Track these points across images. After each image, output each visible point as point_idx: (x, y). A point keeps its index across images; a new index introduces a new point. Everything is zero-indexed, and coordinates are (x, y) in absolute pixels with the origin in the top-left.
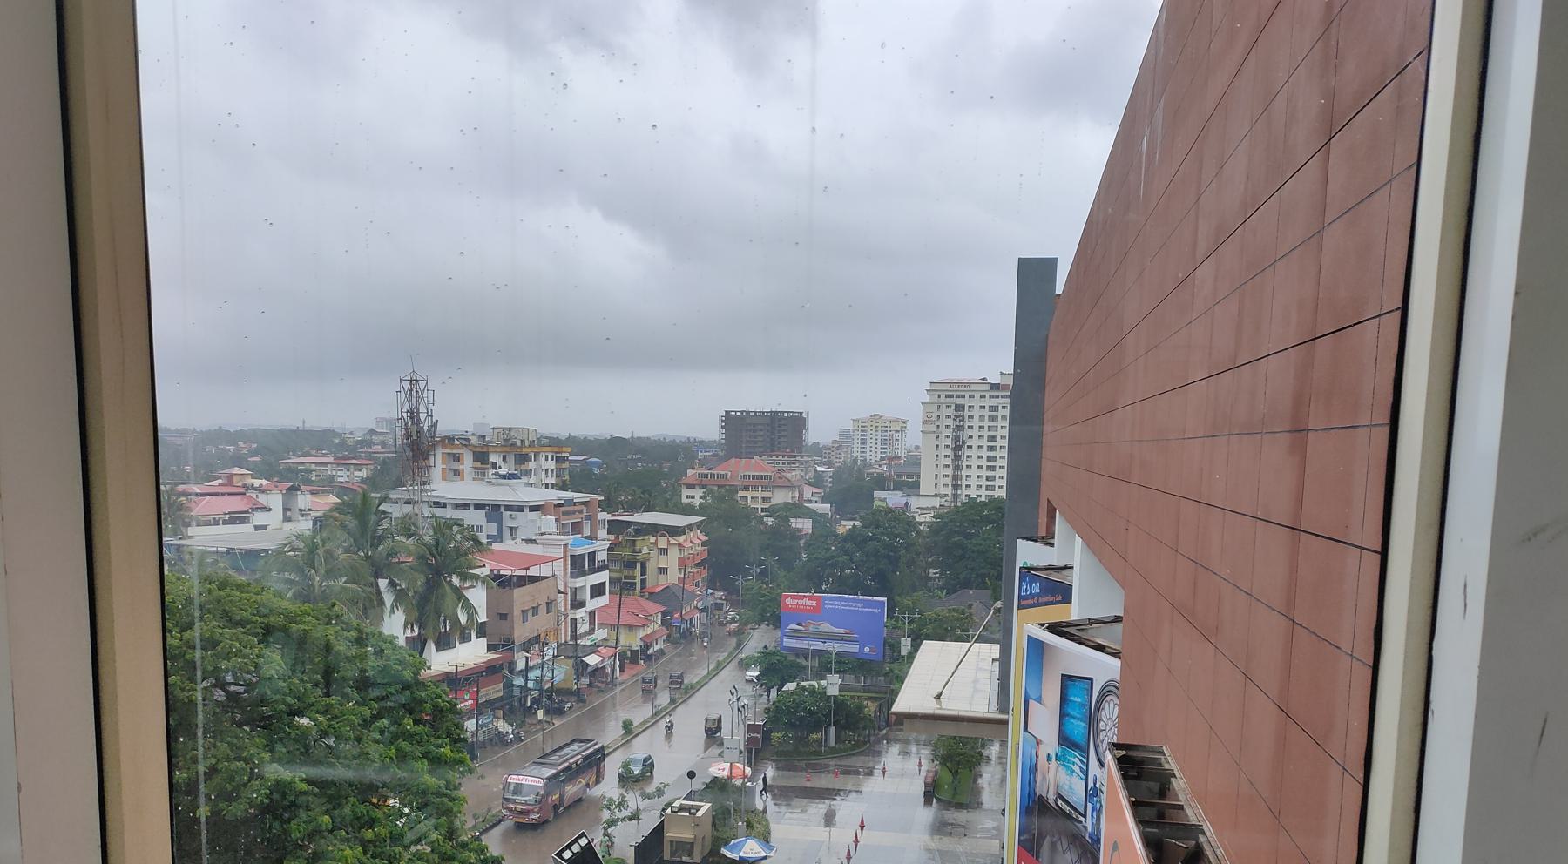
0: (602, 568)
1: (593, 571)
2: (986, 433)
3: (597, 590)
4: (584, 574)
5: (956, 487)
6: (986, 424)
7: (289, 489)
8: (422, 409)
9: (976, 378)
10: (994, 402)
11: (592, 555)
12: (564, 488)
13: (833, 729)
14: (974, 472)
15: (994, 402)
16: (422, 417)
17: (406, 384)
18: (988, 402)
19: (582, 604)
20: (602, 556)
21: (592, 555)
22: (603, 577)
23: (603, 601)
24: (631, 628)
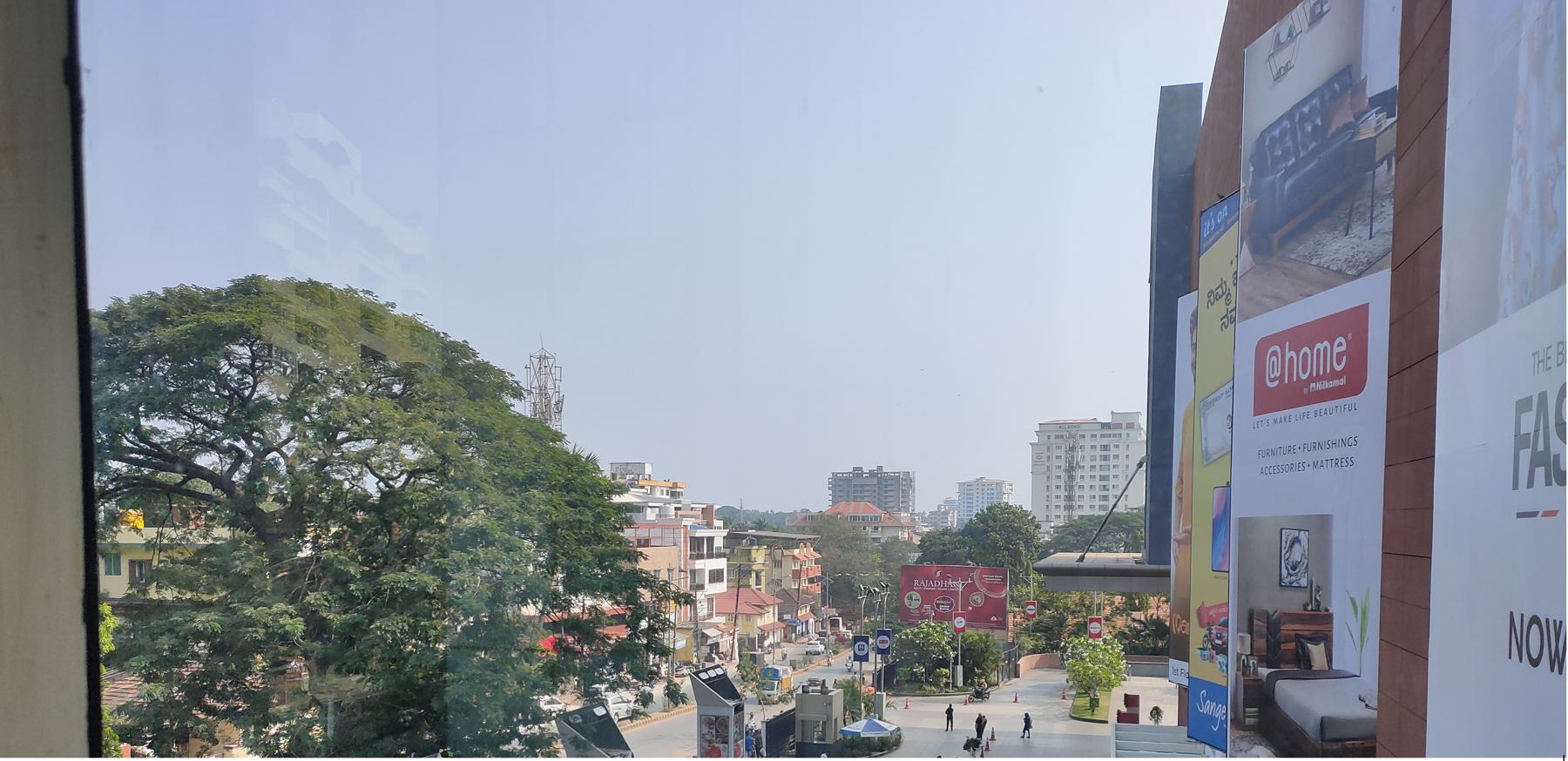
0: (719, 556)
1: (710, 556)
2: (1097, 473)
3: (716, 576)
4: (700, 557)
5: (1069, 508)
6: (1098, 463)
7: (371, 544)
8: (550, 385)
9: (1089, 418)
10: (1105, 441)
11: (711, 540)
12: (582, 732)
13: (960, 668)
14: (1088, 453)
15: (1105, 441)
16: (550, 392)
17: (536, 361)
18: (1100, 442)
19: (701, 587)
20: (719, 543)
21: (711, 540)
22: (721, 564)
23: (721, 587)
24: (748, 616)
